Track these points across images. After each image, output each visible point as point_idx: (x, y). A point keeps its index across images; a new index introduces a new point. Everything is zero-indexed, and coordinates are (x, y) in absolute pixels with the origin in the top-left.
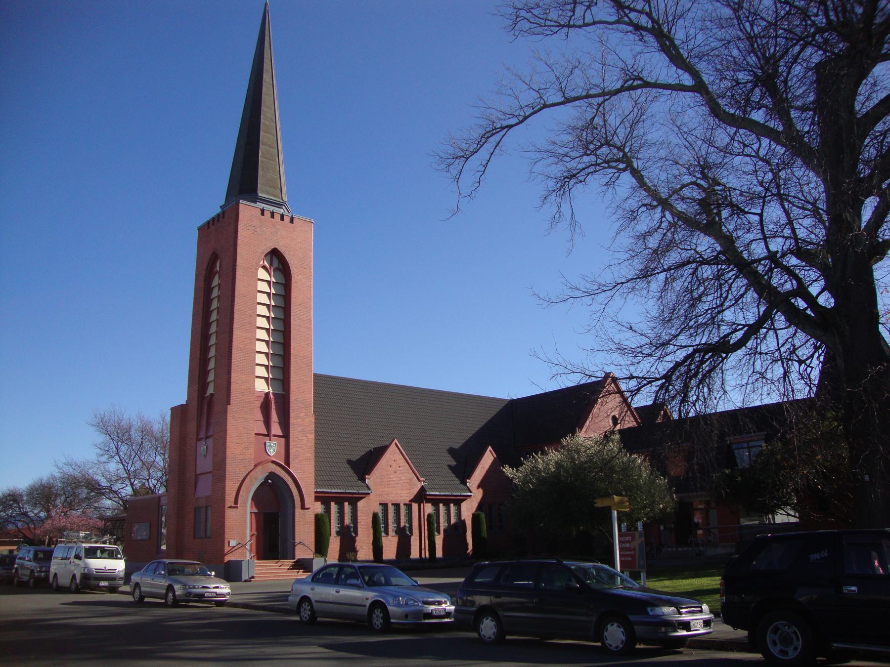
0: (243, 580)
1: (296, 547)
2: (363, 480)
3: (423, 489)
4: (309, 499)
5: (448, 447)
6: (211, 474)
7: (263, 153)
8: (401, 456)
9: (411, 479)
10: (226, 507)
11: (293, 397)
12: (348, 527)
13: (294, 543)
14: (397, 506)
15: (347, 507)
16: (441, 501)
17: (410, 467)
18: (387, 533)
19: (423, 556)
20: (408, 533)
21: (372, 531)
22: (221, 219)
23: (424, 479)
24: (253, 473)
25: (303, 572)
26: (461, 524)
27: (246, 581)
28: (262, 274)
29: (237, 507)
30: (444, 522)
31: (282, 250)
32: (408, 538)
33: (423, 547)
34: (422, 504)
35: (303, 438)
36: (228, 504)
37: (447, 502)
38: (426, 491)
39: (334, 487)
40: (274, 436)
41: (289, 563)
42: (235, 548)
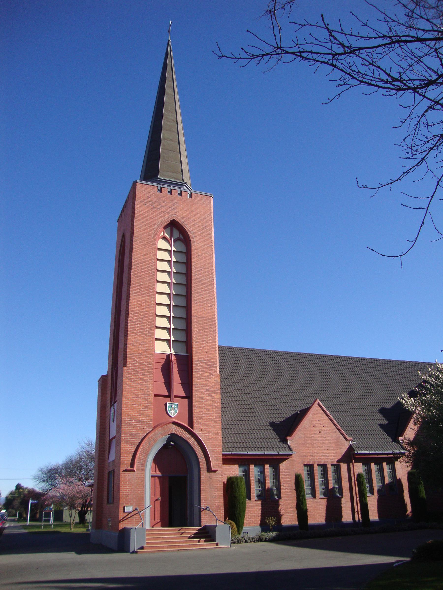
0: (131, 551)
1: (202, 513)
2: (284, 441)
3: (351, 449)
4: (216, 462)
5: (379, 407)
7: (164, 145)
8: (325, 416)
9: (338, 439)
10: (121, 471)
11: (195, 358)
12: (270, 490)
13: (200, 509)
14: (324, 467)
15: (268, 469)
16: (385, 460)
17: (336, 426)
18: (314, 495)
19: (357, 519)
20: (338, 495)
21: (295, 494)
23: (352, 438)
24: (151, 435)
25: (205, 541)
26: (396, 483)
27: (134, 552)
28: (162, 244)
29: (133, 471)
30: (377, 482)
31: (180, 220)
32: (339, 500)
33: (356, 510)
34: (351, 464)
36: (123, 467)
37: (379, 461)
38: (354, 450)
39: (251, 448)
40: (176, 397)
41: (193, 530)
42: (132, 514)
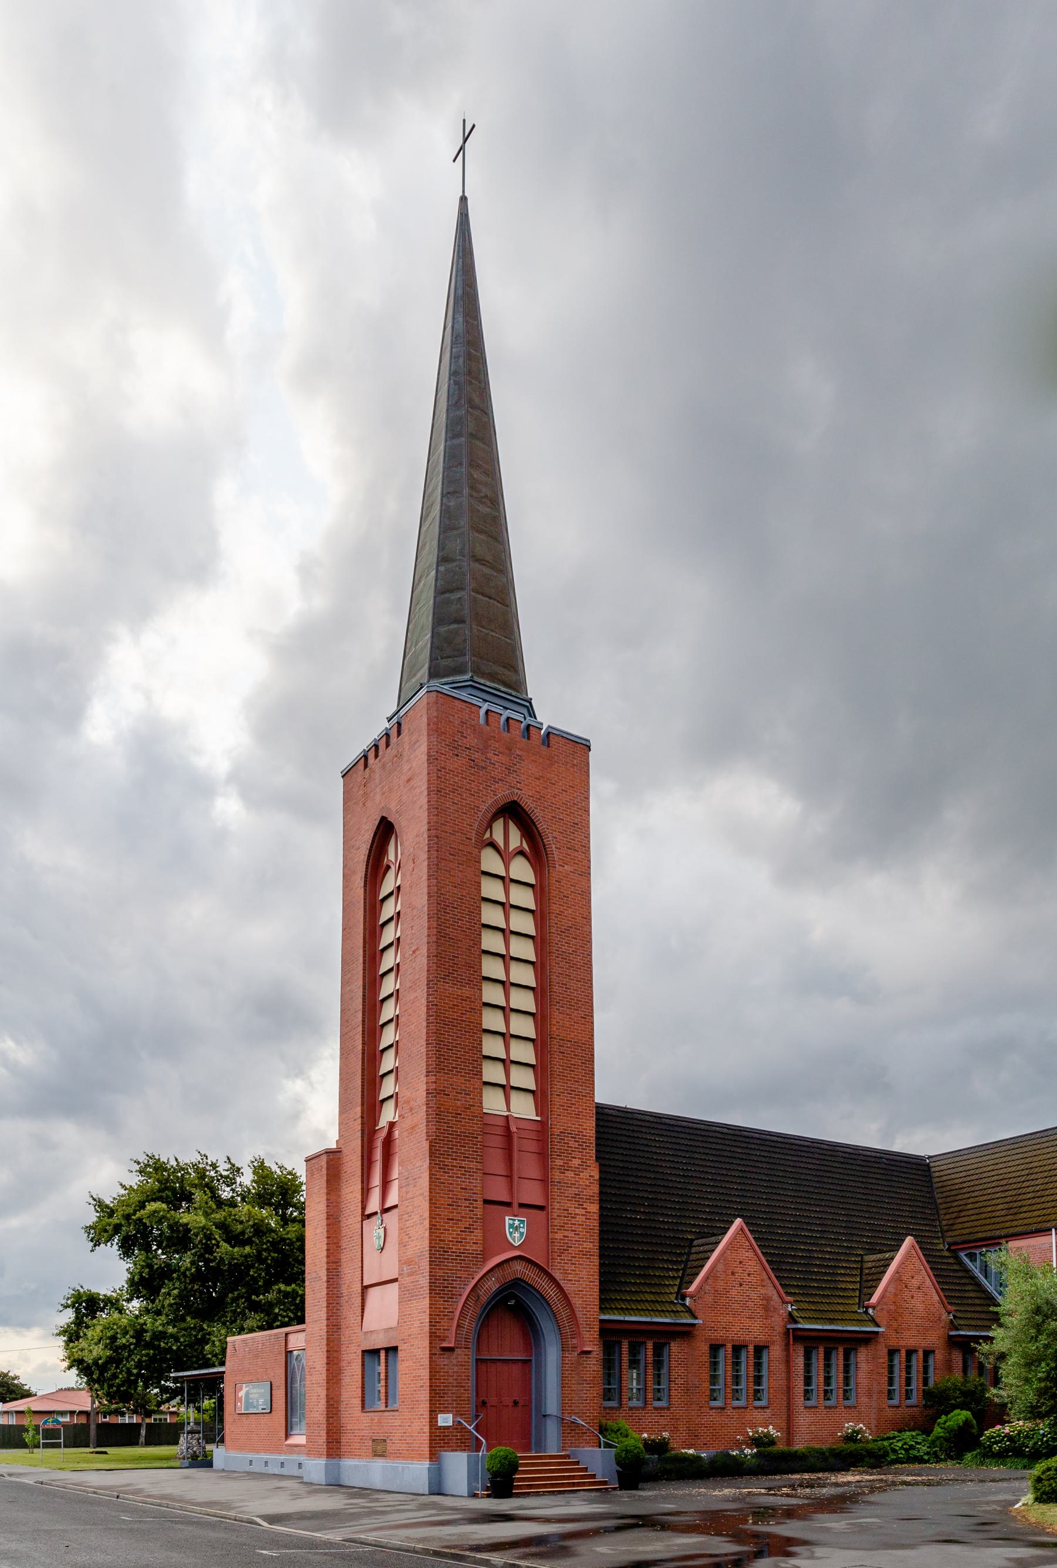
6: (396, 1284)
22: (394, 739)
31: (528, 804)
35: (577, 1211)
